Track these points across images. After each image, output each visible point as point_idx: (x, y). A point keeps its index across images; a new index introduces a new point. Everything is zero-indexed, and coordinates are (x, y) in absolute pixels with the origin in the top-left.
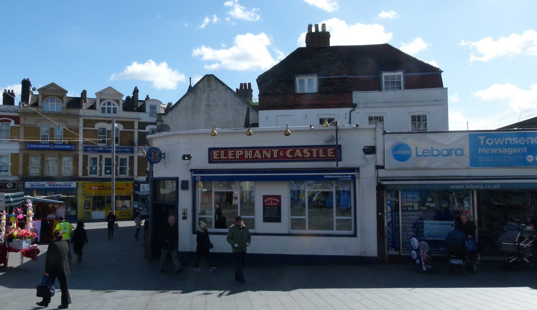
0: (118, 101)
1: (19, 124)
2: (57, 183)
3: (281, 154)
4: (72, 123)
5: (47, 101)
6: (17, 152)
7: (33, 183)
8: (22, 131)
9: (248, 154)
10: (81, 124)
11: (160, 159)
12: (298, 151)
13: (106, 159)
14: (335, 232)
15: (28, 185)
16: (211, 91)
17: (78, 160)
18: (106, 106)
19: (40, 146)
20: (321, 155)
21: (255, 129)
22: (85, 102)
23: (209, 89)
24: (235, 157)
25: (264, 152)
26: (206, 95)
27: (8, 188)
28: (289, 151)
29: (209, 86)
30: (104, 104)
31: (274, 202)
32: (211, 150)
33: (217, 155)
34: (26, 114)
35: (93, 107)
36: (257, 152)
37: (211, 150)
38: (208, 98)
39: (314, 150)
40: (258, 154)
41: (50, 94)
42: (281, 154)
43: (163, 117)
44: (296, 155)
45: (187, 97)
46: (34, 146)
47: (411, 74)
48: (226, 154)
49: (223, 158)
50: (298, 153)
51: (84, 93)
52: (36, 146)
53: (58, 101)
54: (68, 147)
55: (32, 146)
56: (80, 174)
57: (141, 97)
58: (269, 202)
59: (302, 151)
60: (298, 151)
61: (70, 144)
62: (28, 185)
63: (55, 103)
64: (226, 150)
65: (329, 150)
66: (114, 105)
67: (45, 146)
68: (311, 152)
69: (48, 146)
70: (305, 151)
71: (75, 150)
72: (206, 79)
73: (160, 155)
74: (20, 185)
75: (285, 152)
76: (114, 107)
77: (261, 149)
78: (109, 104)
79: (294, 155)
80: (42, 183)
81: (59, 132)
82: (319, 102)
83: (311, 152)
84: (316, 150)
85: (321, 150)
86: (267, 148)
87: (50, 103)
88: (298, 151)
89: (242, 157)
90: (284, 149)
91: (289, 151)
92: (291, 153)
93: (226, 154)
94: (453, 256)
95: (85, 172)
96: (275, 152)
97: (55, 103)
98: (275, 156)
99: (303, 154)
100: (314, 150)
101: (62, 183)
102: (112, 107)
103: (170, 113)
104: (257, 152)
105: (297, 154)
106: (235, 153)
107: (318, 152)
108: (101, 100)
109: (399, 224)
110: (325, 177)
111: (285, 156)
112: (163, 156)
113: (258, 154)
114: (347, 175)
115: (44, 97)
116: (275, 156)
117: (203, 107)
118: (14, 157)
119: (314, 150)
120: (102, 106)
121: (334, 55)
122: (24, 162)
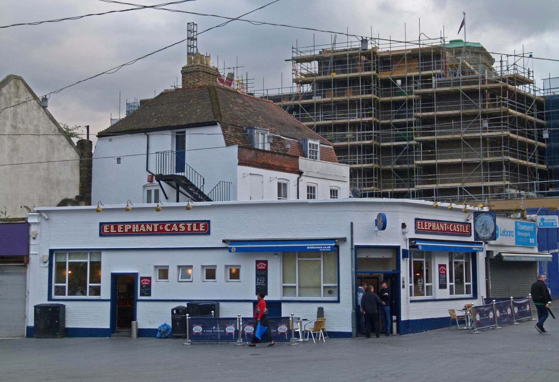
3: (161, 228)
12: (175, 225)
13: (115, 277)
20: (195, 229)
24: (124, 230)
31: (147, 282)
32: (102, 224)
36: (142, 226)
37: (102, 224)
38: (15, 114)
39: (189, 225)
42: (161, 228)
44: (173, 229)
48: (116, 228)
58: (144, 282)
59: (178, 225)
68: (186, 226)
75: (163, 226)
79: (171, 229)
83: (186, 226)
89: (130, 230)
90: (163, 223)
92: (170, 227)
93: (116, 228)
94: (361, 295)
96: (156, 225)
98: (156, 230)
99: (179, 228)
100: (189, 225)
104: (142, 226)
106: (124, 227)
107: (192, 226)
110: (308, 248)
111: (164, 230)
114: (327, 246)
116: (156, 230)
122: (376, 197)
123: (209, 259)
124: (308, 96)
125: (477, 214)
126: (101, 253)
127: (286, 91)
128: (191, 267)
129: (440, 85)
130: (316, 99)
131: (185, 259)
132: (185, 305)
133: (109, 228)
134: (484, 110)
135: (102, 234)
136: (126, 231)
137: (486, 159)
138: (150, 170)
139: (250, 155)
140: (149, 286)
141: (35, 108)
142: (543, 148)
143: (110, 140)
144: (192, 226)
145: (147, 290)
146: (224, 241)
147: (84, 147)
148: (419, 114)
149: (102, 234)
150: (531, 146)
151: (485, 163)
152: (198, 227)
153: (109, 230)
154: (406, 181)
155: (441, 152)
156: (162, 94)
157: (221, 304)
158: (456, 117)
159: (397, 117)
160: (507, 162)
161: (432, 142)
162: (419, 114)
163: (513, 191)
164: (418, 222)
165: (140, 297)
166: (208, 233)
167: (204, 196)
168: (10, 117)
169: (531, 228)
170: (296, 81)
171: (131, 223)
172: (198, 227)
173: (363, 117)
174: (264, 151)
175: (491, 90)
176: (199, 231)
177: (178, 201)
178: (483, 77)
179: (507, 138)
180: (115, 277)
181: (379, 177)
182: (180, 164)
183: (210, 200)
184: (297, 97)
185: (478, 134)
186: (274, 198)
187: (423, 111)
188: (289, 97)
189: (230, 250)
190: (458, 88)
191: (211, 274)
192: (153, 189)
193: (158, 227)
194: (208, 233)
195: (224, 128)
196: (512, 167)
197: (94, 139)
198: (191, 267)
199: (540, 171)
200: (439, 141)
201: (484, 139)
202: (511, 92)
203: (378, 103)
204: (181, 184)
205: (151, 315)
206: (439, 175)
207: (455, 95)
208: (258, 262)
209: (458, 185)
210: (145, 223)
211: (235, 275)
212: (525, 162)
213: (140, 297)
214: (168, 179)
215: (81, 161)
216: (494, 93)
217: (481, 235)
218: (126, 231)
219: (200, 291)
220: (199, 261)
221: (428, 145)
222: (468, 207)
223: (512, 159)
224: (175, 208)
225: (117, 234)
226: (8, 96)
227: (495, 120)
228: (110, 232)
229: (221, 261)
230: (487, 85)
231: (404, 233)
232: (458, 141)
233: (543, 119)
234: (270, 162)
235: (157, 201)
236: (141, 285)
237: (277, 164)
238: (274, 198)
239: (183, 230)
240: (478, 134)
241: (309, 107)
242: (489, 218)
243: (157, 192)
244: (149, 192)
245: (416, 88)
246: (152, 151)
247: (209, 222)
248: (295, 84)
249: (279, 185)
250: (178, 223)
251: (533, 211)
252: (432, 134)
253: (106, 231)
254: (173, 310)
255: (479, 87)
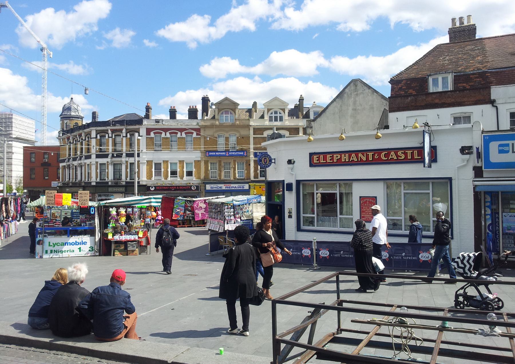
0: (284, 110)
1: (200, 135)
2: (232, 185)
3: (376, 157)
4: (243, 132)
5: (222, 114)
6: (199, 159)
7: (212, 185)
8: (202, 140)
9: (345, 158)
10: (252, 132)
11: (270, 164)
14: (315, 228)
15: (208, 187)
16: (357, 94)
17: (250, 165)
18: (273, 115)
19: (217, 153)
20: (416, 157)
21: (386, 131)
22: (256, 111)
23: (356, 93)
25: (360, 155)
26: (352, 99)
27: (193, 190)
28: (384, 153)
29: (356, 90)
30: (272, 113)
32: (311, 155)
33: (316, 159)
34: (205, 127)
35: (262, 117)
37: (311, 155)
38: (355, 103)
39: (409, 152)
40: (354, 157)
41: (225, 107)
43: (312, 123)
44: (390, 157)
45: (335, 103)
46: (212, 154)
47: (17, 15)
48: (325, 158)
49: (417, 157)
50: (393, 155)
51: (255, 104)
52: (214, 154)
53: (231, 113)
54: (240, 153)
55: (210, 154)
56: (252, 178)
57: (307, 104)
60: (392, 153)
61: (242, 150)
62: (208, 187)
63: (229, 115)
64: (325, 154)
65: (328, 156)
66: (280, 113)
67: (221, 153)
68: (406, 154)
69: (223, 153)
70: (399, 153)
71: (246, 156)
72: (352, 84)
73: (270, 161)
74: (202, 188)
75: (379, 155)
76: (280, 115)
77: (357, 152)
78: (276, 113)
80: (220, 185)
81: (233, 140)
82: (453, 100)
83: (406, 154)
84: (410, 152)
85: (416, 152)
86: (362, 152)
87: (224, 115)
88: (392, 153)
90: (379, 151)
91: (384, 153)
92: (385, 156)
93: (325, 158)
95: (256, 176)
96: (370, 154)
97: (229, 115)
98: (371, 159)
100: (409, 152)
101: (237, 185)
102: (278, 115)
103: (319, 119)
104: (353, 155)
105: (392, 156)
107: (412, 154)
108: (269, 110)
109: (499, 227)
112: (273, 161)
113: (354, 157)
115: (219, 110)
116: (371, 159)
117: (350, 111)
118: (197, 162)
119: (408, 152)
120: (269, 115)
121: (476, 48)
126: (352, 184)
128: (49, 242)
135: (312, 165)
136: (335, 161)
138: (495, 109)
141: (370, 95)
144: (412, 154)
149: (312, 165)
164: (315, 157)
168: (351, 104)
176: (326, 162)
193: (373, 156)
198: (49, 242)
218: (335, 161)
226: (349, 93)
228: (320, 162)
239: (403, 158)
250: (396, 150)
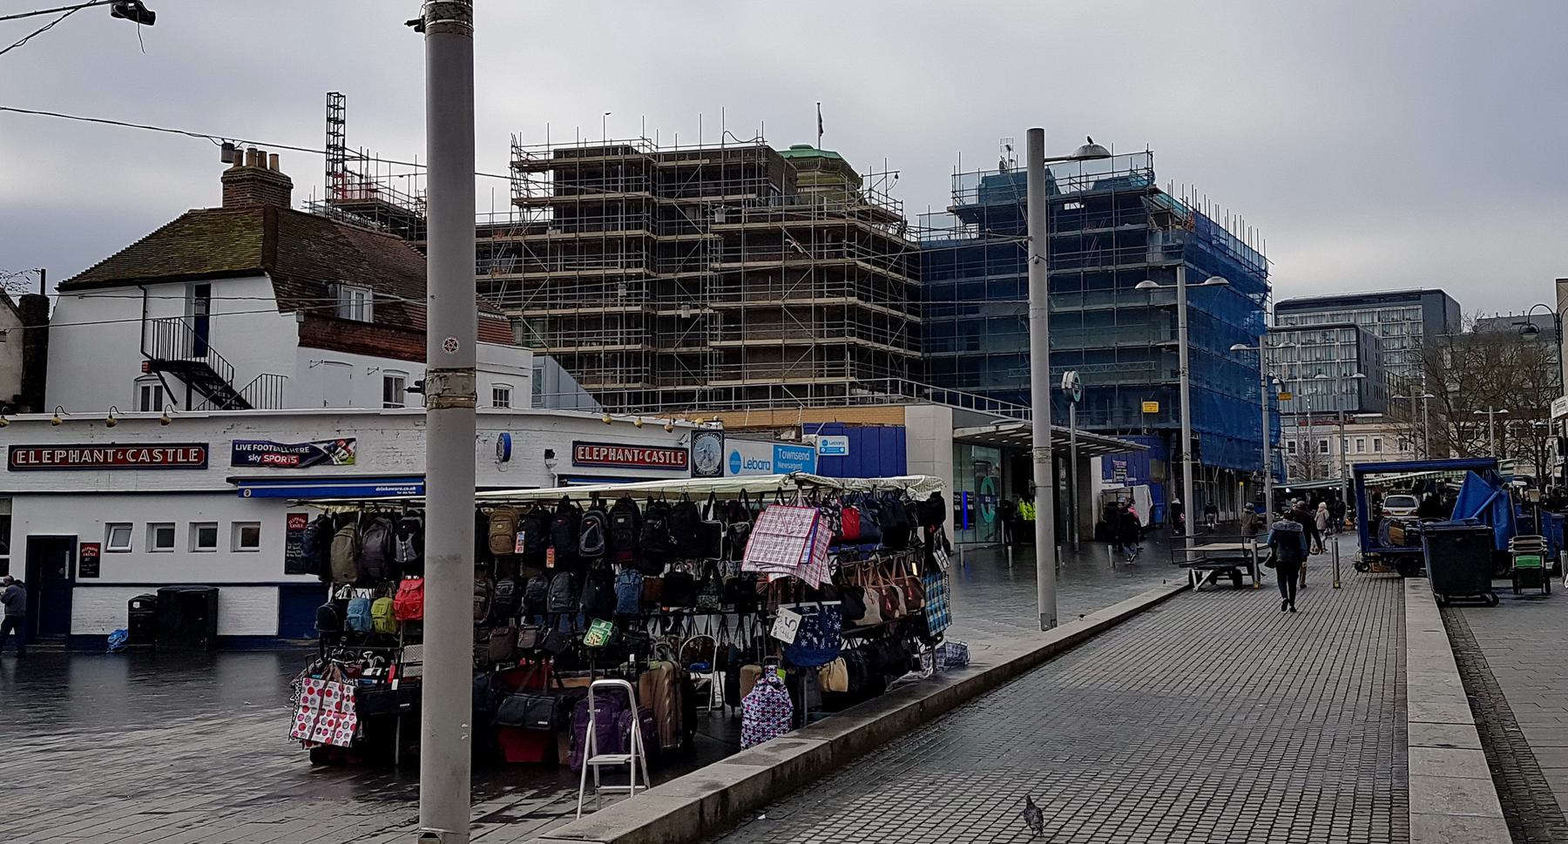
3: (120, 457)
13: (34, 543)
48: (38, 456)
68: (165, 454)
75: (124, 454)
93: (38, 456)
96: (110, 452)
99: (152, 457)
100: (170, 451)
106: (52, 455)
107: (175, 454)
123: (206, 511)
124: (541, 228)
125: (696, 433)
127: (505, 219)
129: (752, 219)
130: (554, 234)
131: (163, 512)
132: (154, 592)
133: (27, 455)
134: (819, 262)
137: (820, 341)
139: (322, 330)
140: (96, 560)
142: (917, 324)
143: (82, 297)
144: (175, 454)
145: (92, 566)
146: (229, 480)
147: (34, 310)
148: (717, 265)
150: (896, 322)
151: (819, 347)
152: (186, 455)
153: (26, 459)
154: (696, 374)
155: (752, 328)
156: (185, 217)
157: (221, 589)
158: (776, 273)
159: (685, 269)
160: (853, 348)
161: (738, 311)
162: (717, 265)
163: (865, 393)
165: (78, 580)
166: (205, 466)
167: (239, 399)
169: (806, 456)
170: (517, 202)
171: (66, 447)
172: (186, 455)
173: (629, 266)
174: (359, 324)
175: (831, 229)
177: (189, 408)
178: (820, 208)
179: (852, 307)
180: (34, 543)
181: (653, 367)
182: (201, 347)
183: (249, 407)
184: (518, 228)
185: (809, 301)
186: (378, 406)
187: (726, 260)
188: (506, 229)
189: (240, 493)
190: (779, 224)
191: (208, 537)
192: (152, 385)
194: (205, 466)
195: (276, 282)
196: (860, 353)
197: (51, 292)
199: (910, 361)
200: (748, 310)
201: (819, 308)
202: (863, 234)
203: (654, 246)
204: (201, 378)
205: (98, 610)
206: (746, 366)
207: (773, 237)
208: (290, 516)
209: (771, 382)
210: (91, 447)
211: (250, 537)
212: (884, 347)
213: (78, 580)
214: (177, 368)
215: (26, 332)
216: (837, 234)
217: (702, 468)
219: (184, 567)
220: (182, 516)
221: (731, 316)
222: (681, 422)
223: (861, 342)
224: (185, 418)
225: (40, 467)
227: (833, 277)
229: (227, 515)
230: (826, 222)
231: (548, 467)
232: (777, 311)
233: (917, 278)
234: (368, 341)
235: (158, 408)
236: (82, 559)
237: (384, 344)
238: (378, 406)
240: (809, 301)
241: (539, 248)
242: (714, 441)
243: (158, 389)
244: (146, 390)
245: (713, 222)
246: (151, 316)
247: (206, 446)
248: (516, 208)
249: (387, 381)
251: (811, 428)
252: (738, 298)
253: (20, 461)
254: (131, 603)
255: (811, 224)
